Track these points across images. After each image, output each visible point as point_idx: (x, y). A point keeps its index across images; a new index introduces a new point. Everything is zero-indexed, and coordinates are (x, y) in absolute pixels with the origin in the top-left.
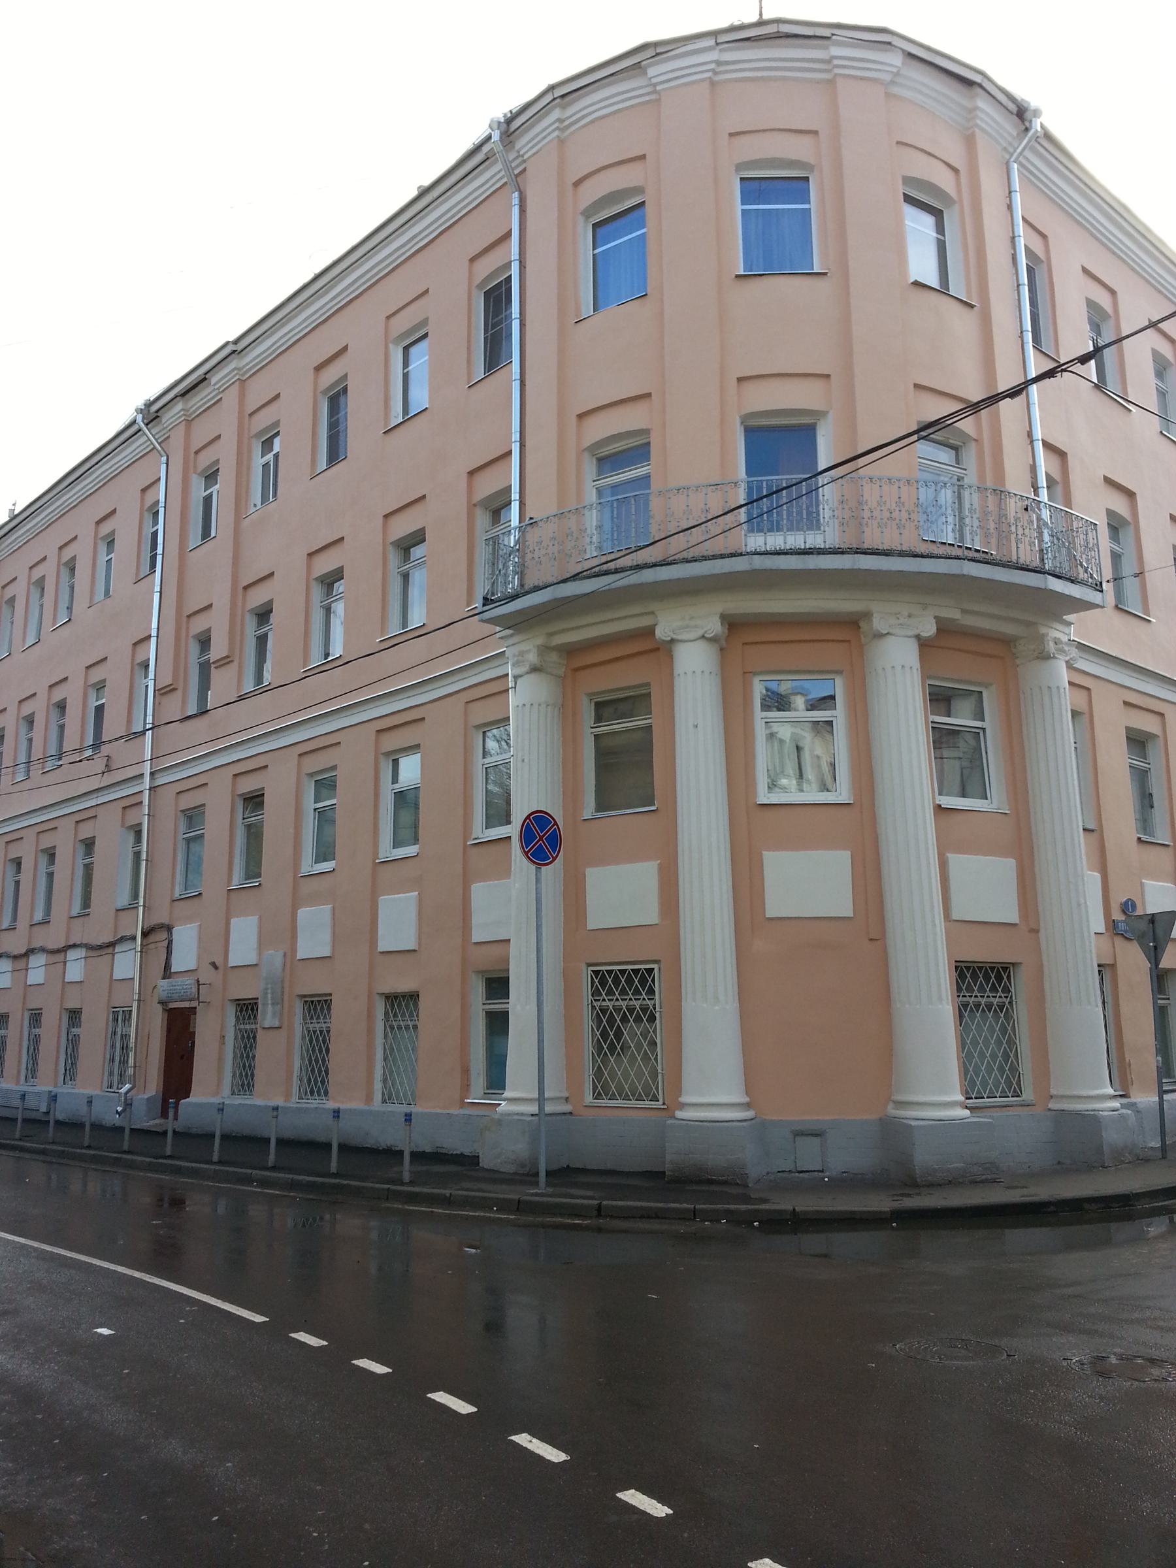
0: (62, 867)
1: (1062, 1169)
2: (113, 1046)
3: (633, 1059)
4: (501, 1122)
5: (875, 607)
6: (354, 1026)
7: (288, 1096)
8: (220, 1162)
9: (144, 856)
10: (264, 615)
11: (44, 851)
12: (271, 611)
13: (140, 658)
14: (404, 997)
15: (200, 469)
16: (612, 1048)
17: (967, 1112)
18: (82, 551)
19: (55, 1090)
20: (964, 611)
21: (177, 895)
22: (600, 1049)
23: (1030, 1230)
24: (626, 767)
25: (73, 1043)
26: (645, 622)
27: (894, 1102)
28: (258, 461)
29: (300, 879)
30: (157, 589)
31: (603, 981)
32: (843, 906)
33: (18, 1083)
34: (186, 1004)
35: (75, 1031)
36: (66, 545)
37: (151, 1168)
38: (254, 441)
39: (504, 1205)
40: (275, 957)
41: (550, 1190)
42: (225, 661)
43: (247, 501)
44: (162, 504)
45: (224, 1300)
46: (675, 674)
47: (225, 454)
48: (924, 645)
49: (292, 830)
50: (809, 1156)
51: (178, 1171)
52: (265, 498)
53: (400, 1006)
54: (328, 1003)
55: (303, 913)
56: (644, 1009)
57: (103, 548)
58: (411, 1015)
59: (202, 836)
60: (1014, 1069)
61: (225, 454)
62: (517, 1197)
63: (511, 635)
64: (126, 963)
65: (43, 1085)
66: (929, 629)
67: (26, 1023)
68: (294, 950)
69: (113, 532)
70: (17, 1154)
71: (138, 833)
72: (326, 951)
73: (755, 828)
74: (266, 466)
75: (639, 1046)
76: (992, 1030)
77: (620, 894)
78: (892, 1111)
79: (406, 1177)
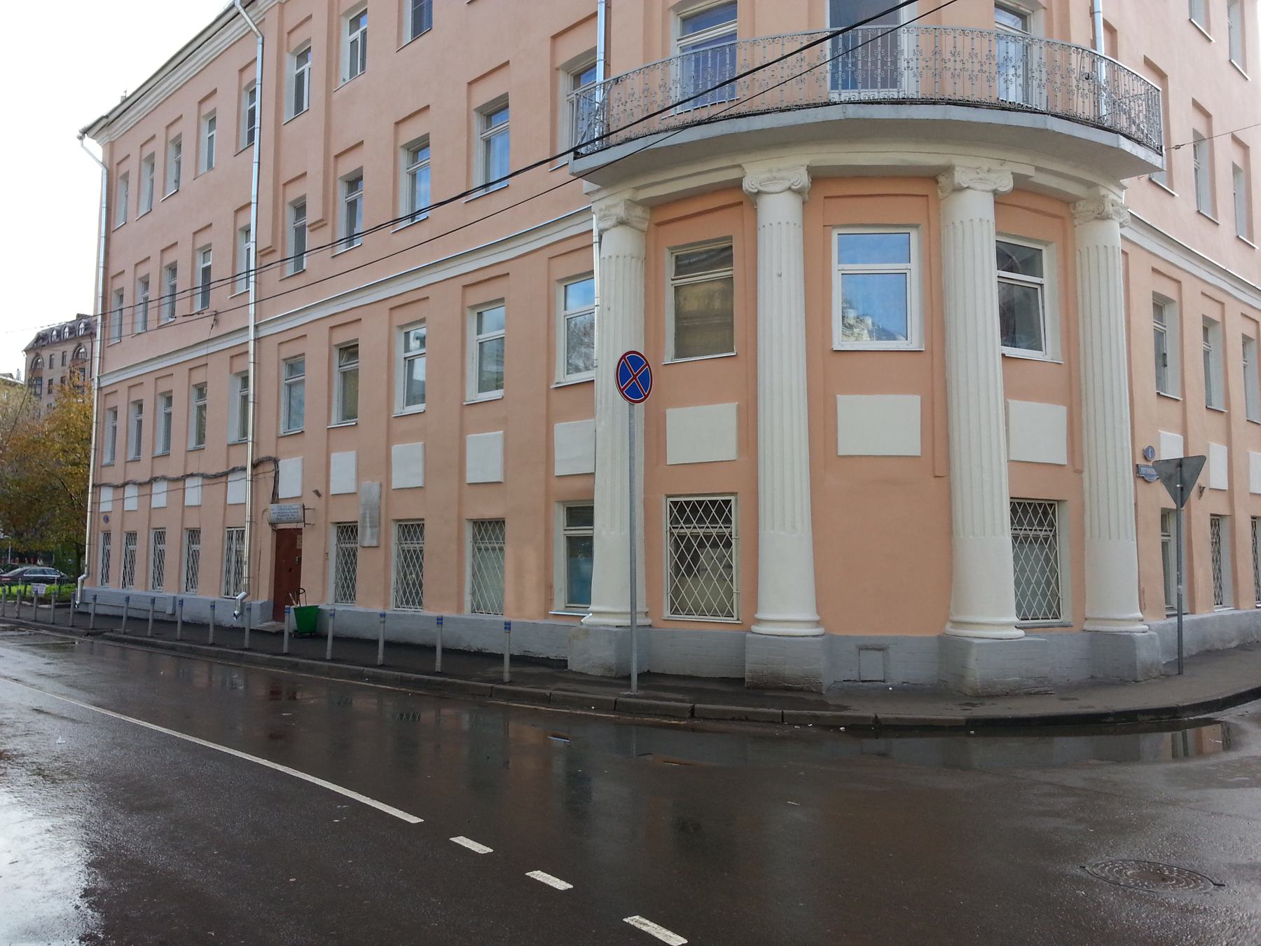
0: (178, 409)
1: (1096, 683)
2: (229, 560)
3: (709, 579)
4: (588, 632)
5: (956, 161)
6: (445, 545)
7: (386, 605)
8: (332, 660)
9: (251, 399)
10: (354, 182)
11: (162, 394)
12: (361, 178)
13: (241, 224)
14: (490, 523)
15: (292, 49)
16: (689, 570)
17: (1021, 633)
18: (187, 129)
19: (181, 596)
20: (1038, 169)
21: (282, 433)
22: (677, 570)
23: (1071, 739)
24: (705, 317)
25: (194, 557)
26: (732, 175)
27: (953, 622)
28: (347, 38)
29: (392, 420)
30: (256, 159)
31: (683, 511)
32: (916, 451)
33: (146, 589)
34: (293, 526)
35: (195, 547)
36: (172, 124)
37: (269, 663)
38: (343, 19)
39: (601, 705)
40: (372, 487)
41: (641, 693)
42: (319, 225)
43: (337, 76)
44: (259, 82)
45: (373, 798)
46: (760, 226)
47: (316, 33)
48: (1000, 200)
49: (385, 376)
50: (872, 668)
51: (295, 666)
52: (353, 73)
53: (486, 530)
54: (421, 527)
55: (396, 449)
56: (721, 537)
57: (205, 125)
58: (497, 538)
59: (303, 381)
60: (1055, 595)
61: (316, 33)
62: (613, 698)
63: (598, 190)
64: (239, 490)
65: (169, 590)
66: (1006, 184)
67: (152, 541)
68: (389, 480)
69: (215, 110)
70: (150, 649)
71: (245, 380)
72: (418, 482)
73: (830, 373)
74: (354, 43)
75: (715, 569)
76: (1037, 559)
77: (699, 433)
78: (949, 629)
79: (507, 677)
